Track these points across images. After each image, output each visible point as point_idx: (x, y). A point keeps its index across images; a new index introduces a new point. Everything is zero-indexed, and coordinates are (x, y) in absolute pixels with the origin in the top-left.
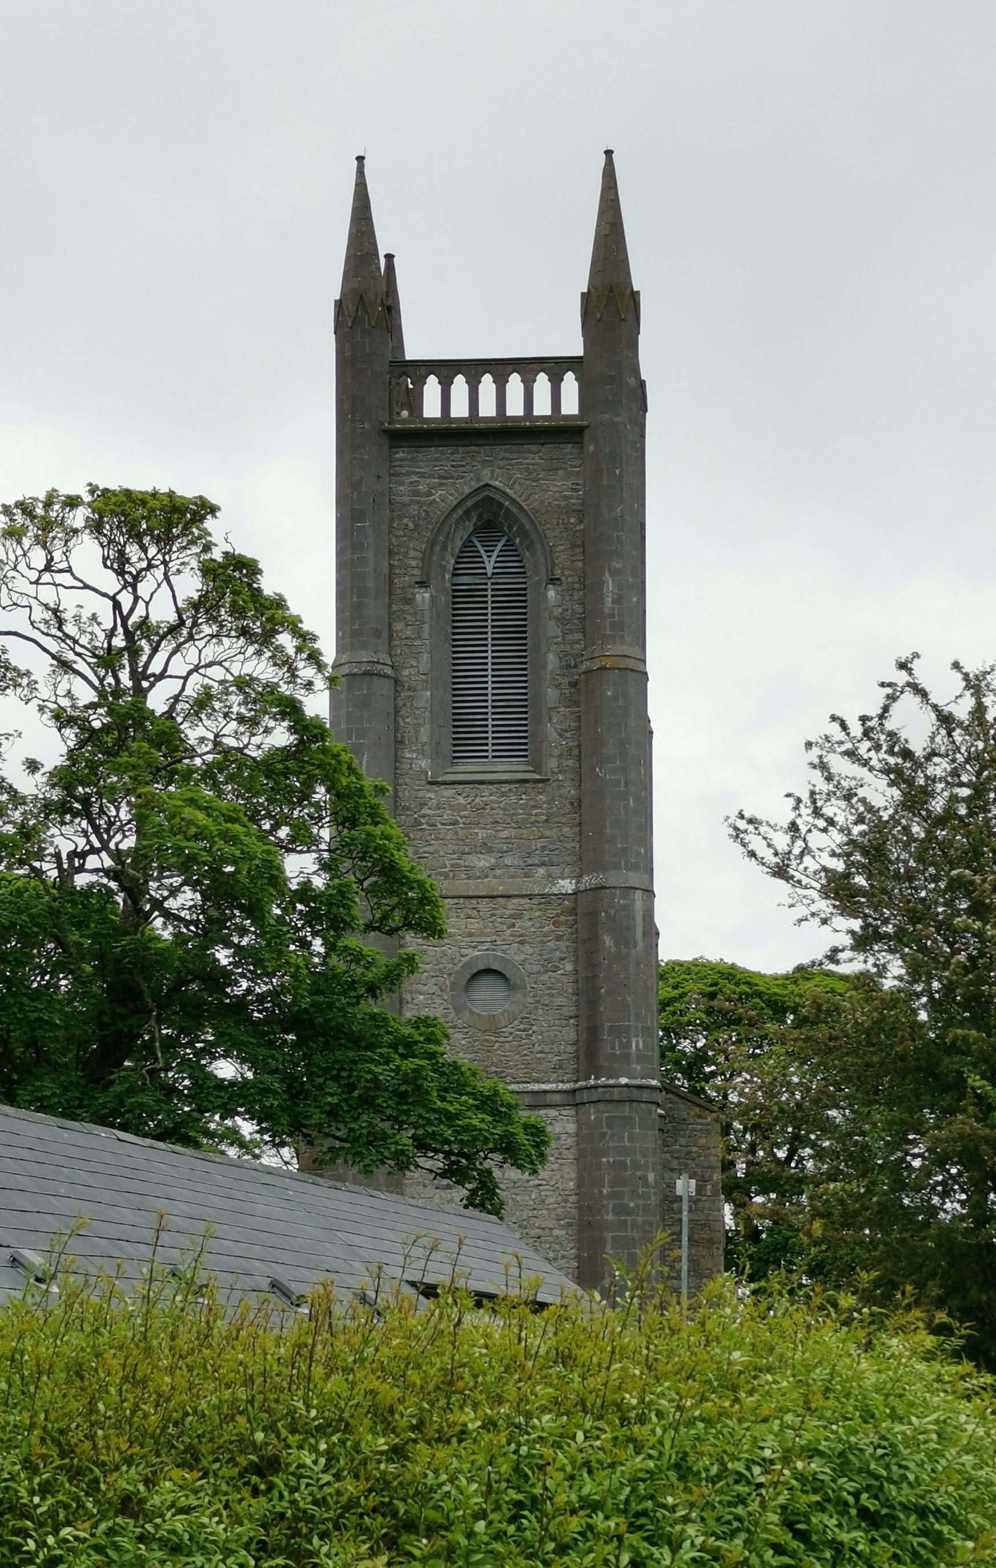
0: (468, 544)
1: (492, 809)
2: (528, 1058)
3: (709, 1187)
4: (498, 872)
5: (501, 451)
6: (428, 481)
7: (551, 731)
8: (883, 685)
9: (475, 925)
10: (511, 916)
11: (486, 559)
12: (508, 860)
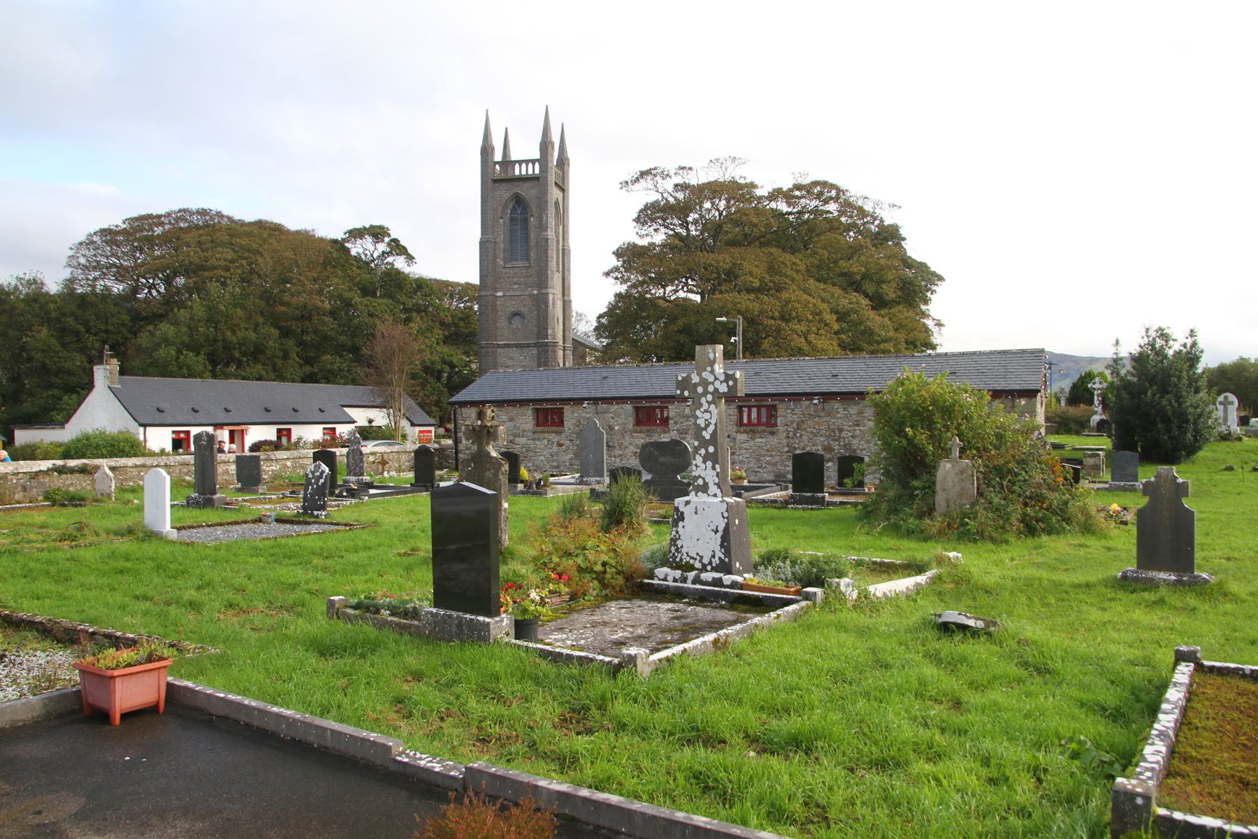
0: (514, 207)
5: (520, 183)
8: (607, 274)
9: (514, 303)
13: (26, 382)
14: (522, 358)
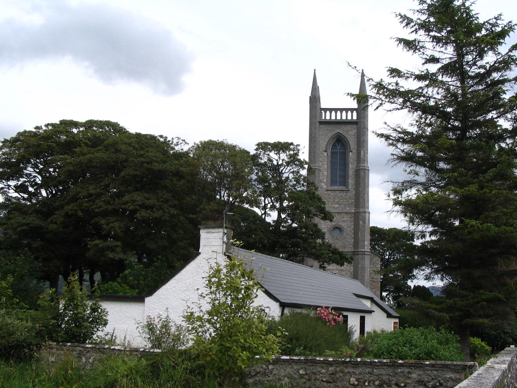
7: (350, 181)
12: (341, 206)
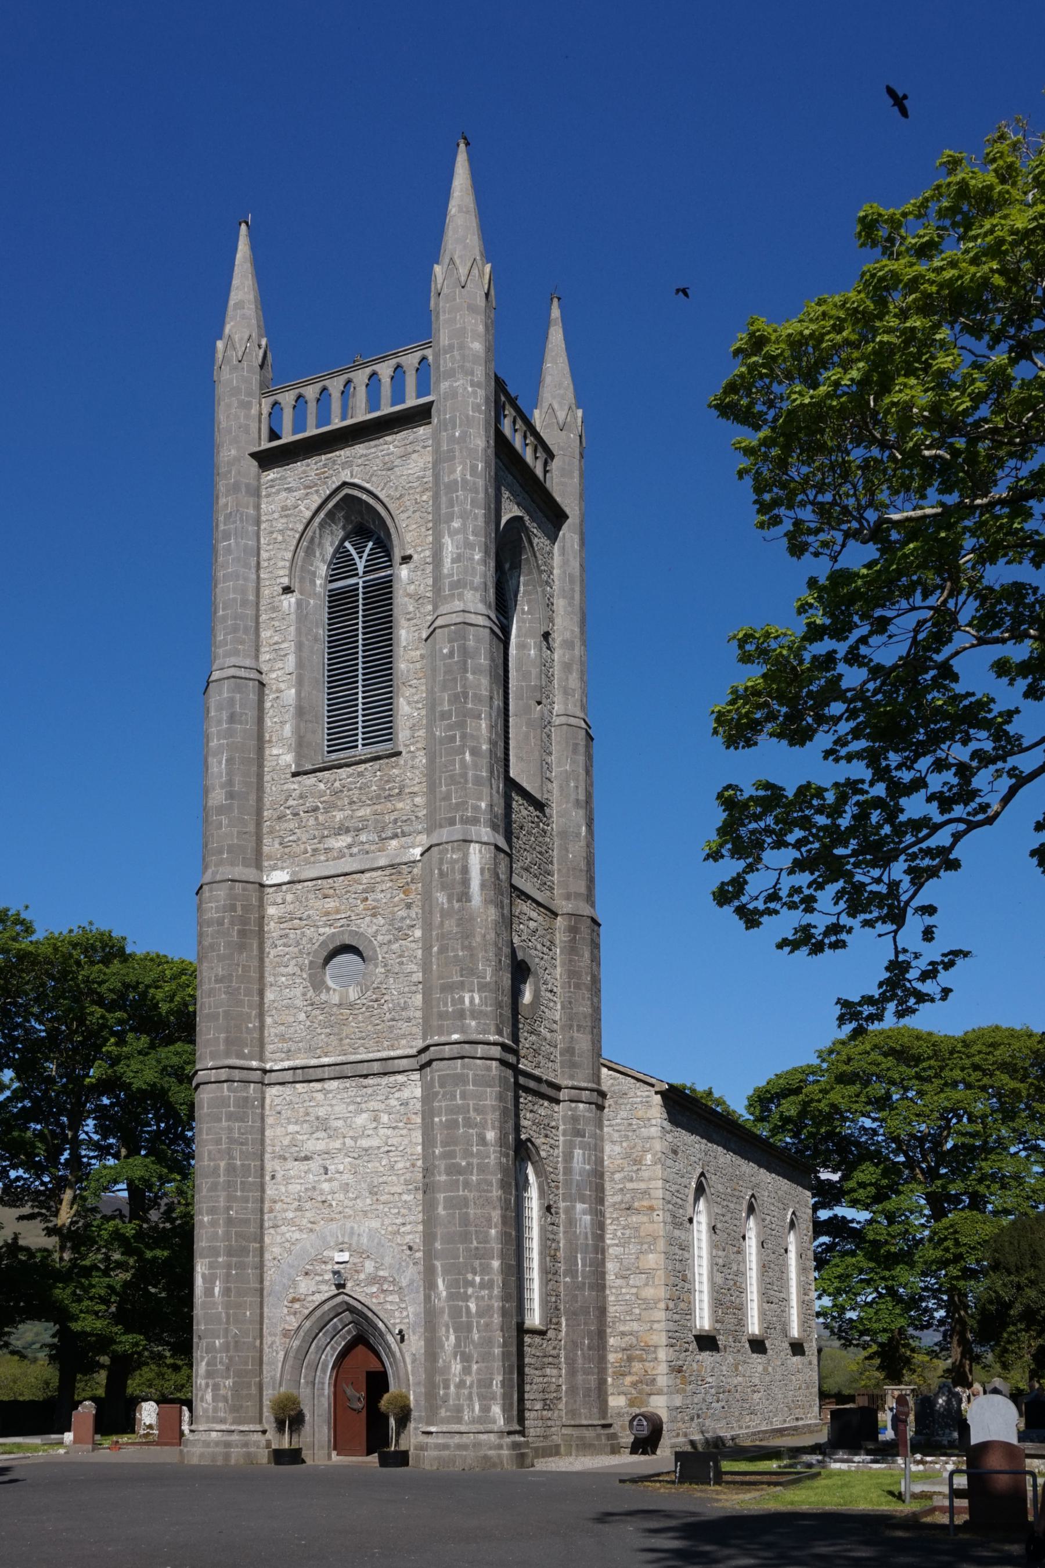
1: (350, 790)
2: (379, 1027)
3: (649, 1157)
4: (355, 850)
6: (295, 494)
9: (331, 904)
10: (365, 891)
11: (357, 560)
12: (363, 838)
13: (17, 1056)
14: (362, 1119)
